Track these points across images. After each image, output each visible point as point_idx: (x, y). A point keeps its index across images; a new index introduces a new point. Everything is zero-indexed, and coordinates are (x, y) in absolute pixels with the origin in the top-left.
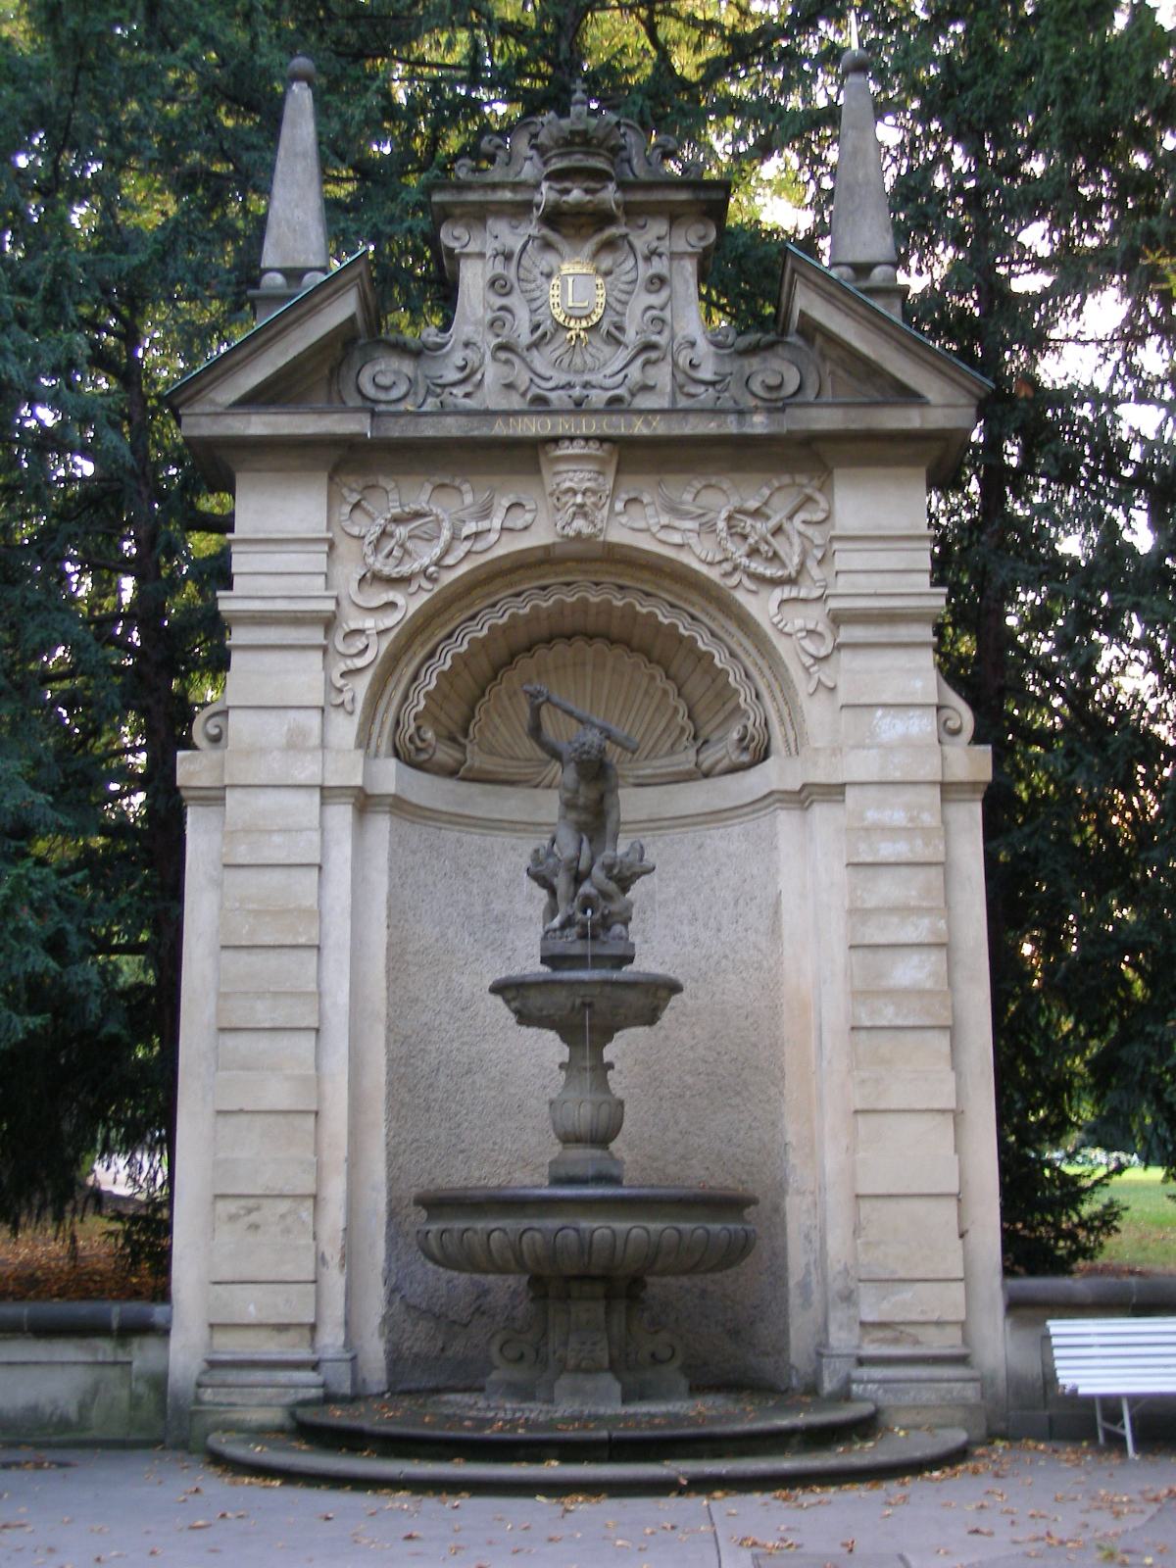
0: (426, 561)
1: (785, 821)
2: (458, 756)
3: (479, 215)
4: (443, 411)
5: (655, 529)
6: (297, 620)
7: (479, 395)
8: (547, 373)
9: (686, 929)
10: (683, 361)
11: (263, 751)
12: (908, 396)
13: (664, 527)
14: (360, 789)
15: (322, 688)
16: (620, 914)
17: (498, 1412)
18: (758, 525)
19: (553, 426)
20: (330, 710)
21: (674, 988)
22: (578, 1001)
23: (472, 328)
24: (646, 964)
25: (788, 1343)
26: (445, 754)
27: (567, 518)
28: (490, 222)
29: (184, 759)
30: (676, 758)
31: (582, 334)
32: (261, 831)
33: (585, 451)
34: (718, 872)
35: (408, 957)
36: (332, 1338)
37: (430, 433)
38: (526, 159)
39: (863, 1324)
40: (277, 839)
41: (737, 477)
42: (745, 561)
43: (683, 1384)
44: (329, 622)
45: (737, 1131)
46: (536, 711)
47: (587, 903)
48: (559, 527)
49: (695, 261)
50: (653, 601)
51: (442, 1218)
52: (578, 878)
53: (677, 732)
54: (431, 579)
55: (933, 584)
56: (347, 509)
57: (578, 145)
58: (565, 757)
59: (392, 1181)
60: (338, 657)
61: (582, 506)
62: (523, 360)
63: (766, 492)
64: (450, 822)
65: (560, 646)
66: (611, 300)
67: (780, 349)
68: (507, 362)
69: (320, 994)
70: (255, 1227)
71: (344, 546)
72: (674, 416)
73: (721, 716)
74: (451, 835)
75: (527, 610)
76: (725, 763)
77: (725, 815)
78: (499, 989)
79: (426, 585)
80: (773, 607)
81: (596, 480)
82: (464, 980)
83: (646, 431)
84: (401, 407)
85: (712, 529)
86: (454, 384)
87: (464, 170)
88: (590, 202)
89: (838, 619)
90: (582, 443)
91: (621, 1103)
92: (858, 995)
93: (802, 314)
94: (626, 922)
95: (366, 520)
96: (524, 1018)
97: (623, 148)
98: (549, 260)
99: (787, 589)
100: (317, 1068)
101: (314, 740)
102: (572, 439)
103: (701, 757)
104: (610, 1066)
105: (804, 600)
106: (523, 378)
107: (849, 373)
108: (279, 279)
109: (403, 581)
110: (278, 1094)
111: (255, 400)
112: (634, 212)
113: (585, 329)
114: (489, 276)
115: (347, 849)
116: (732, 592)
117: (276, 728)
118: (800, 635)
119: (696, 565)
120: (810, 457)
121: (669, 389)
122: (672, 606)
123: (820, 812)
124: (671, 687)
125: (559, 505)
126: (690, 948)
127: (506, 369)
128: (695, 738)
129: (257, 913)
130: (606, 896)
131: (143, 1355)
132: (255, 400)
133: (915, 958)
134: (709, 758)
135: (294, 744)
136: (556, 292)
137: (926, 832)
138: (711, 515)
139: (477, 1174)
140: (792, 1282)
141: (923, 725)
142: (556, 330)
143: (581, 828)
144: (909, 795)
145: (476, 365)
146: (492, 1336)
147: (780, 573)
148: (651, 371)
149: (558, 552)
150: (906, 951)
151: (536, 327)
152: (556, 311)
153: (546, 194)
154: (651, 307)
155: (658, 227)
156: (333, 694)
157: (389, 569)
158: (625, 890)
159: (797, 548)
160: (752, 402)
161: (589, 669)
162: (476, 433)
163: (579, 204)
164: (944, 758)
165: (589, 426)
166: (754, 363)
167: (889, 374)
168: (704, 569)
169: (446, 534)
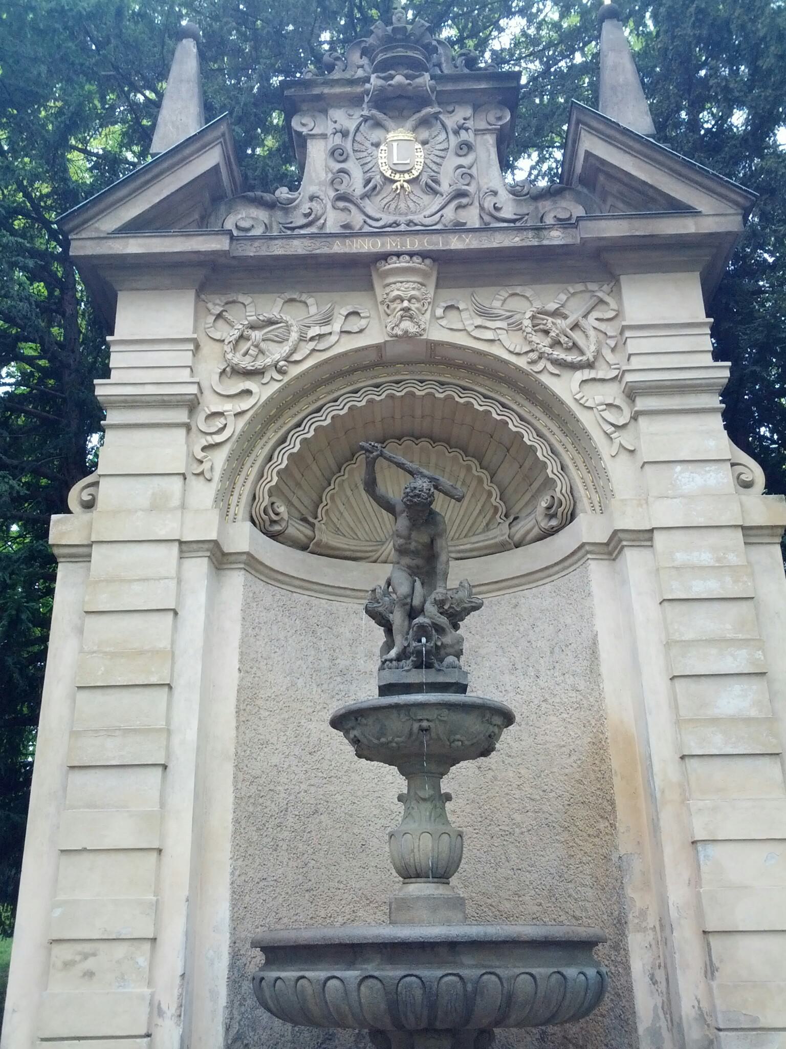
0: (277, 357)
1: (596, 570)
2: (309, 532)
3: (321, 105)
5: (469, 329)
6: (164, 403)
8: (377, 216)
14: (215, 542)
15: (184, 458)
16: (452, 646)
18: (558, 321)
19: (383, 245)
20: (192, 480)
21: (508, 718)
22: (416, 726)
23: (317, 187)
24: (481, 689)
26: (297, 530)
27: (396, 321)
28: (331, 112)
29: (58, 521)
30: (491, 534)
31: (406, 185)
32: (122, 581)
33: (411, 264)
35: (259, 702)
40: (136, 587)
41: (538, 287)
44: (192, 405)
46: (371, 465)
47: (423, 630)
48: (389, 328)
49: (494, 136)
52: (412, 613)
54: (281, 372)
55: (716, 358)
56: (211, 319)
58: (399, 507)
59: (236, 921)
60: (200, 435)
61: (407, 310)
63: (563, 297)
66: (428, 161)
67: (567, 194)
69: (169, 732)
71: (208, 348)
73: (527, 497)
74: (301, 598)
76: (536, 531)
78: (339, 722)
79: (278, 376)
80: (575, 386)
81: (419, 290)
82: (312, 726)
88: (409, 84)
89: (631, 393)
90: (408, 258)
91: (460, 835)
92: (679, 722)
93: (586, 152)
94: (459, 654)
95: (226, 327)
96: (364, 751)
99: (586, 371)
100: (162, 805)
101: (176, 502)
102: (398, 255)
103: (514, 530)
104: (448, 797)
105: (603, 380)
110: (121, 833)
111: (135, 227)
112: (448, 100)
113: (408, 182)
114: (329, 147)
115: (202, 597)
116: (538, 376)
117: (141, 493)
118: (600, 408)
119: (506, 356)
120: (601, 265)
122: (485, 397)
123: (632, 557)
124: (485, 475)
125: (389, 312)
126: (511, 694)
128: (506, 516)
129: (113, 655)
130: (440, 630)
132: (135, 227)
134: (521, 529)
135: (157, 506)
136: (383, 155)
138: (517, 317)
139: (323, 914)
140: (641, 1030)
141: (720, 478)
142: (384, 184)
143: (413, 572)
144: (714, 538)
145: (320, 213)
147: (579, 358)
149: (389, 353)
151: (368, 182)
152: (384, 168)
153: (375, 81)
155: (462, 113)
156: (195, 465)
157: (246, 363)
158: (456, 627)
162: (318, 251)
163: (400, 85)
164: (742, 505)
165: (412, 244)
168: (513, 359)
169: (294, 336)
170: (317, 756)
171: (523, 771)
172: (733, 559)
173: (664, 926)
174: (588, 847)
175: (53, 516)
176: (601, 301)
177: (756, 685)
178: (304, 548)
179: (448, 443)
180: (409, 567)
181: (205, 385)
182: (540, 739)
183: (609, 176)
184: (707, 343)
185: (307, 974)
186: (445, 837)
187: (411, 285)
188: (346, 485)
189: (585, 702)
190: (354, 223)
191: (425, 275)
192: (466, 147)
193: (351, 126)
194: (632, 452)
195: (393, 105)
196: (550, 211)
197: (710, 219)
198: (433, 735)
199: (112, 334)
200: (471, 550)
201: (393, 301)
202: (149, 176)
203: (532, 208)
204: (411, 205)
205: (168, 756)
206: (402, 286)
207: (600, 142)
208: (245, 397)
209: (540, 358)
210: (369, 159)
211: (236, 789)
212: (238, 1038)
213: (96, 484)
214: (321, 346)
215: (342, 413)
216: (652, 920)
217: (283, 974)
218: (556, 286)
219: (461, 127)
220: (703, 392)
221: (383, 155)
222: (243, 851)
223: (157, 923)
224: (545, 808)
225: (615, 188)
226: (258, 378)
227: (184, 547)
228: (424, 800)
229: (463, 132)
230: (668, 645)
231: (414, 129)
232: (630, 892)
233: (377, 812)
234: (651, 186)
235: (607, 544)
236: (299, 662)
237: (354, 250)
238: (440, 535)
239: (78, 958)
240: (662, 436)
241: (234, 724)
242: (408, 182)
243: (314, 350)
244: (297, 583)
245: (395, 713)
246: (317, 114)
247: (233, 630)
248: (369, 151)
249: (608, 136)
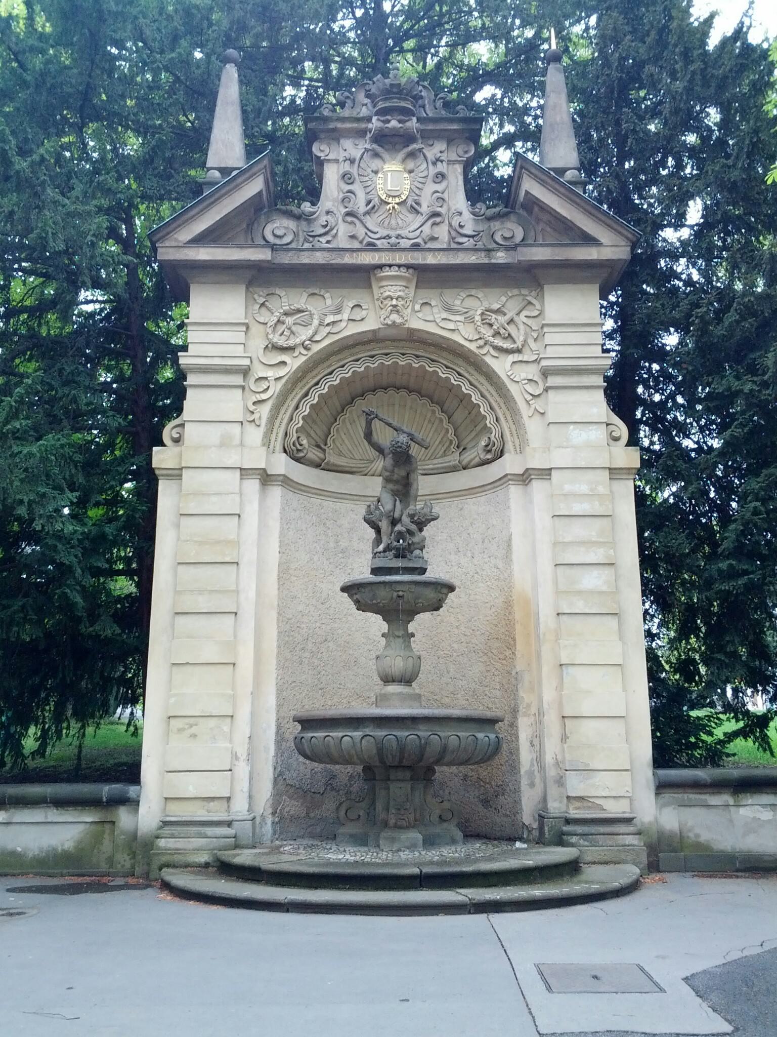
0: (304, 338)
1: (514, 491)
2: (322, 456)
3: (335, 136)
4: (313, 249)
8: (375, 230)
9: (453, 557)
10: (455, 223)
12: (589, 240)
14: (264, 470)
18: (499, 318)
21: (451, 588)
22: (395, 594)
25: (521, 809)
26: (314, 454)
27: (387, 314)
28: (342, 141)
29: (158, 451)
30: (447, 459)
31: (396, 206)
33: (398, 273)
34: (472, 524)
36: (240, 807)
37: (306, 261)
38: (363, 105)
39: (568, 797)
40: (214, 499)
41: (486, 290)
42: (491, 339)
43: (459, 835)
44: (245, 372)
46: (369, 423)
47: (400, 535)
49: (462, 166)
50: (436, 364)
51: (310, 733)
52: (394, 522)
53: (447, 444)
54: (307, 348)
57: (394, 93)
58: (387, 451)
59: (279, 706)
63: (504, 299)
64: (316, 494)
65: (380, 393)
66: (413, 187)
67: (512, 217)
68: (351, 223)
69: (237, 592)
70: (194, 736)
71: (255, 329)
72: (451, 252)
73: (473, 434)
74: (316, 501)
76: (477, 460)
78: (344, 589)
79: (304, 352)
84: (290, 246)
85: (471, 320)
86: (320, 236)
87: (327, 110)
89: (546, 373)
90: (397, 268)
91: (419, 658)
92: (558, 592)
95: (268, 313)
96: (361, 606)
97: (421, 97)
98: (376, 164)
99: (516, 355)
100: (235, 637)
101: (237, 441)
102: (390, 266)
103: (462, 457)
104: (413, 635)
106: (361, 231)
107: (554, 230)
108: (217, 174)
109: (291, 349)
110: (211, 653)
111: (200, 240)
112: (428, 136)
113: (397, 204)
114: (341, 172)
115: (256, 505)
117: (214, 433)
118: (524, 382)
120: (531, 277)
121: (446, 239)
122: (447, 367)
123: (537, 486)
124: (444, 417)
127: (351, 227)
130: (411, 533)
131: (123, 817)
132: (200, 240)
133: (595, 572)
134: (467, 457)
135: (224, 444)
137: (600, 496)
138: (471, 313)
139: (329, 703)
140: (523, 771)
141: (599, 434)
143: (395, 493)
144: (590, 475)
146: (340, 804)
148: (436, 228)
149: (381, 335)
151: (369, 202)
153: (375, 123)
154: (438, 192)
155: (440, 146)
156: (249, 414)
157: (282, 342)
158: (421, 530)
159: (522, 332)
161: (397, 407)
162: (333, 262)
163: (394, 128)
165: (400, 259)
166: (496, 225)
167: (579, 228)
168: (467, 344)
169: (316, 322)
170: (327, 605)
171: (460, 616)
172: (601, 489)
173: (540, 713)
174: (498, 666)
175: (154, 448)
176: (530, 303)
177: (608, 571)
178: (318, 466)
179: (420, 393)
180: (392, 491)
181: (254, 357)
182: (472, 597)
185: (331, 734)
186: (411, 659)
187: (399, 288)
188: (347, 421)
190: (358, 235)
191: (408, 280)
193: (357, 154)
194: (543, 414)
195: (387, 141)
196: (499, 230)
197: (609, 248)
198: (405, 600)
200: (432, 469)
201: (385, 299)
202: (212, 200)
203: (486, 226)
204: (400, 222)
205: (238, 607)
206: (393, 288)
207: (538, 185)
209: (485, 344)
210: (370, 183)
211: (279, 627)
212: (281, 774)
213: (182, 425)
214: (335, 330)
215: (347, 376)
216: (534, 710)
217: (315, 735)
218: (497, 290)
219: (438, 160)
221: (381, 182)
222: (282, 666)
223: (234, 706)
224: (473, 641)
225: (545, 217)
226: (290, 352)
227: (243, 472)
228: (399, 637)
229: (439, 163)
230: (555, 544)
232: (521, 693)
233: (364, 641)
235: (523, 475)
236: (315, 545)
237: (359, 262)
238: (413, 471)
239: (186, 727)
240: (561, 404)
241: (276, 587)
242: (397, 204)
243: (329, 333)
244: (314, 491)
245: (382, 585)
246: (331, 142)
247: (275, 526)
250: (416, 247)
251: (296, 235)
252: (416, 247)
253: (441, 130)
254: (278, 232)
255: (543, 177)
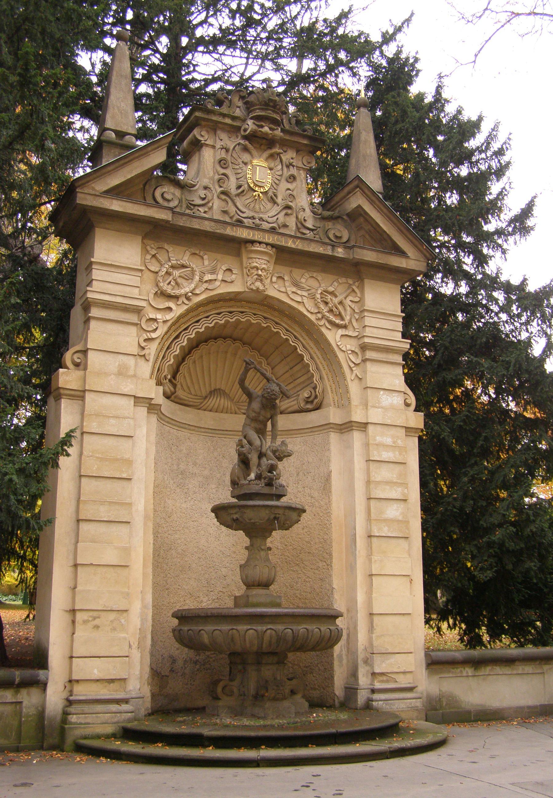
0: (187, 290)
1: (334, 437)
2: (172, 389)
3: (214, 128)
5: (290, 293)
6: (125, 308)
7: (210, 213)
8: (244, 210)
11: (107, 374)
12: (402, 253)
13: (293, 292)
17: (226, 724)
22: (272, 516)
28: (219, 132)
29: (64, 373)
31: (261, 195)
40: (113, 421)
45: (297, 583)
46: (247, 371)
48: (248, 284)
54: (188, 299)
62: (233, 201)
64: (168, 422)
68: (225, 200)
70: (97, 627)
72: (306, 241)
75: (223, 322)
77: (293, 432)
79: (186, 302)
83: (293, 246)
89: (364, 348)
98: (246, 157)
99: (344, 330)
102: (260, 243)
106: (232, 210)
107: (372, 238)
108: (113, 135)
111: (115, 192)
112: (284, 144)
117: (112, 363)
119: (306, 313)
120: (357, 272)
122: (287, 330)
123: (357, 436)
127: (223, 204)
129: (102, 459)
131: (29, 699)
132: (115, 192)
135: (122, 373)
138: (313, 291)
141: (397, 400)
144: (393, 431)
145: (210, 198)
147: (342, 322)
150: (392, 502)
153: (250, 125)
154: (289, 189)
157: (169, 290)
160: (327, 241)
162: (218, 231)
163: (266, 134)
165: (269, 239)
166: (329, 225)
169: (197, 278)
183: (366, 220)
184: (399, 327)
189: (317, 503)
192: (292, 178)
194: (360, 379)
195: (258, 142)
199: (93, 257)
202: (126, 160)
206: (261, 261)
208: (168, 312)
209: (322, 317)
214: (210, 287)
220: (396, 353)
225: (367, 227)
229: (291, 167)
231: (267, 159)
234: (388, 235)
235: (341, 425)
237: (238, 235)
248: (241, 166)
249: (372, 200)
250: (273, 230)
251: (180, 201)
252: (273, 230)
253: (294, 142)
254: (166, 195)
255: (373, 198)
